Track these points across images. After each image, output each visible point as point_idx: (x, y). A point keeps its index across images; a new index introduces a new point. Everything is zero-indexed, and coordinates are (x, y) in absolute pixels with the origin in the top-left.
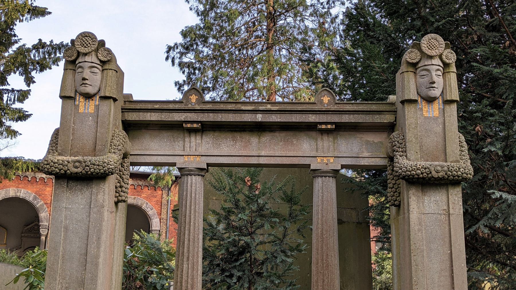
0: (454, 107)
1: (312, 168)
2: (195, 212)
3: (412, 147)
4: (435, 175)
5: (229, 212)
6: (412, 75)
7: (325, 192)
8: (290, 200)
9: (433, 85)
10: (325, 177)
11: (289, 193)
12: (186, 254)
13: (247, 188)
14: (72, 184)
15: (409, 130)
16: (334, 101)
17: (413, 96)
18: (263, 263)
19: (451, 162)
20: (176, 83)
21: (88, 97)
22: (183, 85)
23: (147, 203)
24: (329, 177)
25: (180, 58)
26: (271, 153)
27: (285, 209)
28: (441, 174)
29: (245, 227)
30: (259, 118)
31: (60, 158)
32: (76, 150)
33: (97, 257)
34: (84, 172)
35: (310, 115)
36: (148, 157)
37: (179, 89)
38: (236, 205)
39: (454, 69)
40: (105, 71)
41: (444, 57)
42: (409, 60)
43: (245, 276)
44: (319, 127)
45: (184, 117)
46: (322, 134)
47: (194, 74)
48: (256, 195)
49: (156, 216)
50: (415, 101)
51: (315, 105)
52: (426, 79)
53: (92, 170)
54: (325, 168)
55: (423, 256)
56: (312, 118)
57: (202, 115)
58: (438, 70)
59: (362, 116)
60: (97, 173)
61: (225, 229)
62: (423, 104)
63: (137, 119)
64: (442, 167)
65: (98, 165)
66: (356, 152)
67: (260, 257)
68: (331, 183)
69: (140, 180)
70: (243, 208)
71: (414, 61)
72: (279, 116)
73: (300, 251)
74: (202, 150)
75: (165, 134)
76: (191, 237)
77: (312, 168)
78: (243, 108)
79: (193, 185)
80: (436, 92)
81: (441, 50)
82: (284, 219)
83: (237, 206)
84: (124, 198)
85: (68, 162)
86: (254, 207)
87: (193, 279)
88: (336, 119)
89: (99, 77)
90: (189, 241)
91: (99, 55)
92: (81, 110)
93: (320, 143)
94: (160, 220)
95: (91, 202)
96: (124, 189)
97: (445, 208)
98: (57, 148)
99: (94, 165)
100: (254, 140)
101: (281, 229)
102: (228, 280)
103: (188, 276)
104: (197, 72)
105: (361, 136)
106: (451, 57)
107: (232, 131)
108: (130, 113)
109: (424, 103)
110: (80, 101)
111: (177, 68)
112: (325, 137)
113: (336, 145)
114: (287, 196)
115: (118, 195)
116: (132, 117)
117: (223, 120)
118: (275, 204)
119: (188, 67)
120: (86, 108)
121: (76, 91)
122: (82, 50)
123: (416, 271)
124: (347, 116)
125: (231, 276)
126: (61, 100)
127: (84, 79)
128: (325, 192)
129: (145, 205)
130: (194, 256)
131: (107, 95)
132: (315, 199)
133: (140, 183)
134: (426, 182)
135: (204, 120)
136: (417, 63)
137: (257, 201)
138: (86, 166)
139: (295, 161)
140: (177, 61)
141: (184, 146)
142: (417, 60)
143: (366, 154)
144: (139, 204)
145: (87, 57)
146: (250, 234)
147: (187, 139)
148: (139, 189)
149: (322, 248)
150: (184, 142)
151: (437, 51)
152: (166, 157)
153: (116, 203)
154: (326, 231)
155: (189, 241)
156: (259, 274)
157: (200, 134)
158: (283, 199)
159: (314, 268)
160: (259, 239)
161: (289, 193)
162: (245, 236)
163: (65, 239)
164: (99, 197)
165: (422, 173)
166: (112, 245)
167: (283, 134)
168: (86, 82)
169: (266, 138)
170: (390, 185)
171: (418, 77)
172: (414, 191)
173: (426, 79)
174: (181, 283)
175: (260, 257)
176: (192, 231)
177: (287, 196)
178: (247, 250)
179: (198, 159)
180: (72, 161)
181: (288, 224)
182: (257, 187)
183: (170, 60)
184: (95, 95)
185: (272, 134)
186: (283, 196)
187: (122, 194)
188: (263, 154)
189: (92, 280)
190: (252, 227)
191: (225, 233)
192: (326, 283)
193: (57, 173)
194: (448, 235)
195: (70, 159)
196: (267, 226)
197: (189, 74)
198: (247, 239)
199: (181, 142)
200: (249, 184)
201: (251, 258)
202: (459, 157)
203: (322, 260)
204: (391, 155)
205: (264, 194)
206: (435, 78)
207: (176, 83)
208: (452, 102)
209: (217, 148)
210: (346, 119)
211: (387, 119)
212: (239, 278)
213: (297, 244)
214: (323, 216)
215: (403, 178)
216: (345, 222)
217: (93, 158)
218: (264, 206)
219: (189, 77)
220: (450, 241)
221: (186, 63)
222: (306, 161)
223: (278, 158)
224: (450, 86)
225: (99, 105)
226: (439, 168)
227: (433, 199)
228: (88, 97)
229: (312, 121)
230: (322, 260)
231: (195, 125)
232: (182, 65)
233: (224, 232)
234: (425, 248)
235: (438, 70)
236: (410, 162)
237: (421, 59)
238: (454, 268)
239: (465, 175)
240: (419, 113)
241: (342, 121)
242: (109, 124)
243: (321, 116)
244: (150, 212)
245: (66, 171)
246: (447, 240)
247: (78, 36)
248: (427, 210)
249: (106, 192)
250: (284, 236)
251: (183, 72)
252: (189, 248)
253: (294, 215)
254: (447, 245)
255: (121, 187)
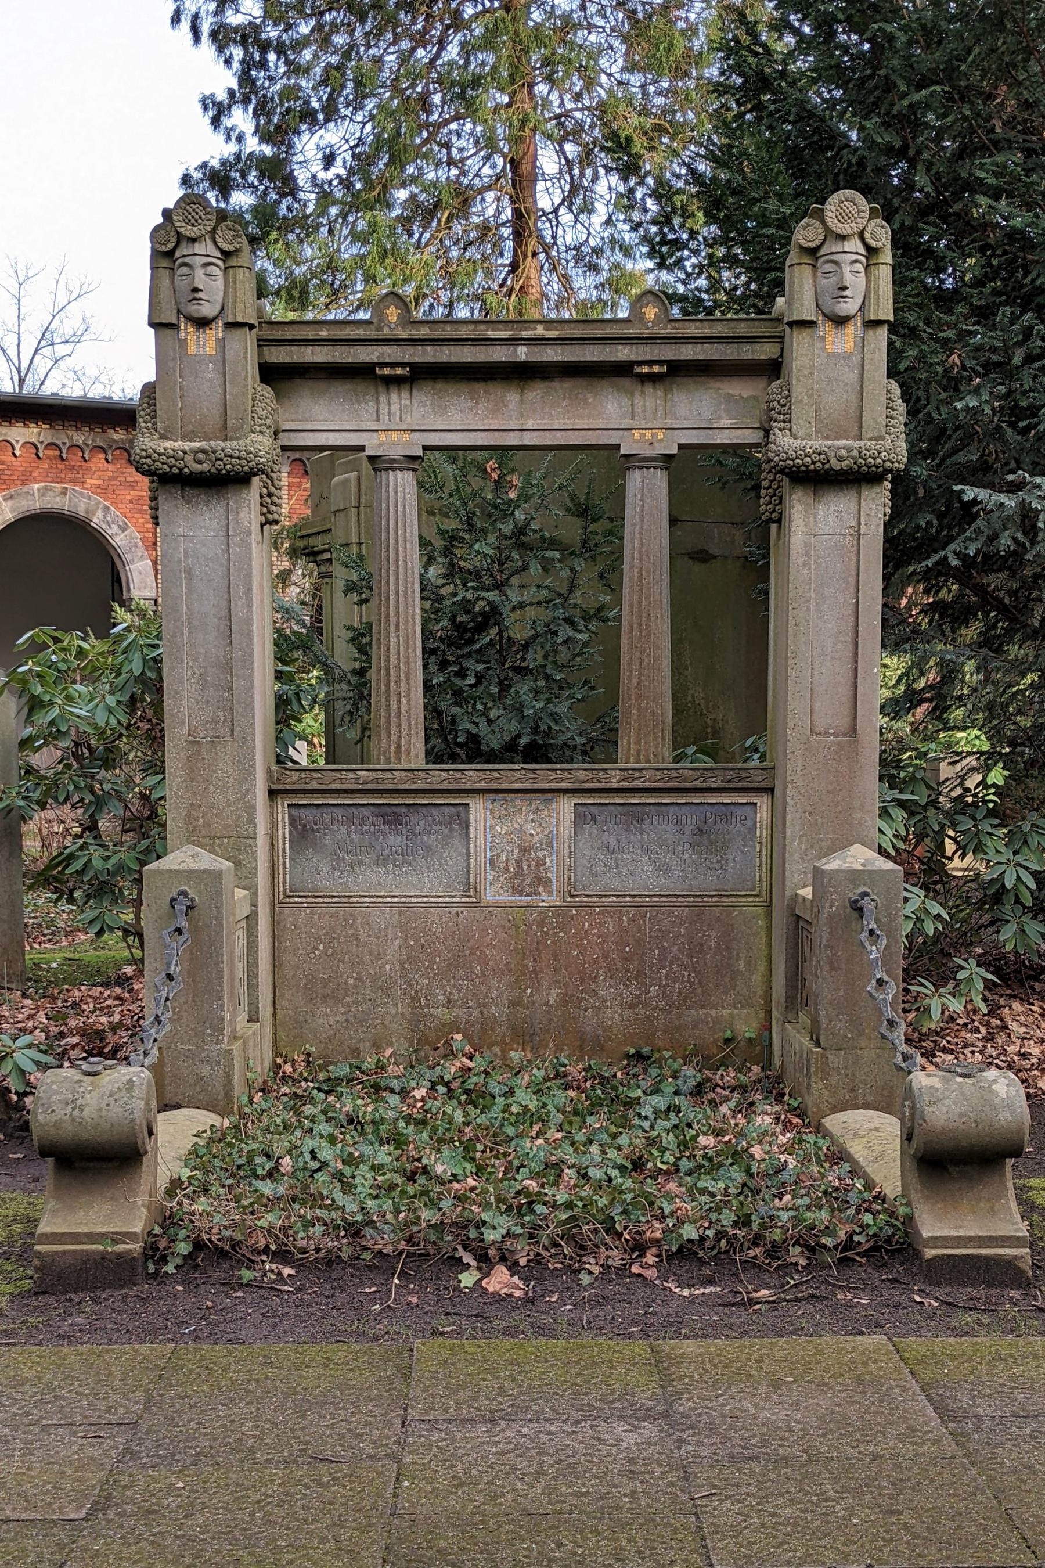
0: (883, 332)
1: (623, 451)
2: (405, 541)
3: (802, 414)
4: (836, 465)
5: (453, 538)
6: (807, 270)
7: (647, 497)
8: (583, 511)
9: (845, 293)
10: (648, 468)
11: (583, 499)
12: (393, 620)
13: (491, 485)
14: (190, 492)
15: (798, 380)
16: (666, 316)
17: (808, 313)
18: (526, 647)
19: (870, 439)
20: (207, 102)
21: (202, 323)
22: (230, 107)
23: (106, 509)
24: (655, 468)
25: (216, 14)
26: (546, 423)
27: (571, 530)
28: (846, 462)
29: (488, 570)
30: (522, 353)
31: (168, 444)
32: (190, 428)
33: (249, 622)
34: (213, 470)
35: (620, 347)
36: (311, 434)
37: (216, 122)
38: (469, 524)
39: (887, 257)
40: (231, 271)
41: (867, 235)
42: (802, 242)
43: (490, 672)
44: (638, 370)
45: (377, 354)
46: (642, 383)
47: (263, 65)
48: (511, 500)
49: (141, 550)
50: (811, 324)
51: (629, 325)
52: (833, 280)
53: (228, 467)
54: (647, 451)
55: (809, 609)
56: (623, 353)
57: (411, 350)
58: (856, 261)
59: (720, 346)
60: (238, 473)
61: (445, 576)
62: (826, 328)
63: (288, 360)
64: (849, 450)
65: (239, 458)
66: (706, 416)
67: (519, 633)
68: (659, 480)
69: (78, 429)
70: (484, 531)
71: (812, 245)
72: (559, 349)
73: (605, 620)
74: (412, 420)
75: (342, 387)
76: (401, 588)
77: (623, 451)
78: (491, 334)
79: (400, 489)
80: (849, 306)
81: (861, 223)
82: (572, 553)
83: (471, 527)
84: (276, 516)
85: (185, 453)
86: (507, 528)
87: (407, 663)
88: (669, 353)
89: (220, 282)
90: (397, 594)
91: (218, 239)
92: (192, 349)
93: (638, 401)
94: (155, 563)
95: (228, 524)
96: (275, 499)
97: (854, 523)
98: (155, 424)
99: (231, 457)
100: (512, 397)
101: (565, 574)
102: (457, 681)
103: (398, 659)
104: (272, 57)
105: (718, 385)
106: (881, 234)
107: (469, 379)
108: (273, 349)
109: (829, 326)
110: (188, 332)
111: (207, 47)
112: (649, 389)
113: (669, 404)
114: (577, 504)
115: (265, 510)
116: (279, 356)
117: (453, 359)
118: (555, 521)
119: (243, 42)
120: (202, 345)
121: (179, 312)
122: (187, 231)
123: (795, 636)
124: (690, 346)
125: (462, 674)
126: (152, 331)
127: (196, 290)
128: (647, 497)
129: (100, 513)
130: (407, 621)
131: (240, 319)
132: (628, 512)
133: (79, 438)
134: (821, 479)
135: (417, 360)
136: (818, 248)
137: (513, 513)
138: (218, 459)
139: (591, 438)
140: (205, 29)
141: (377, 411)
142: (817, 243)
143: (726, 422)
144: (81, 511)
145: (197, 245)
146: (498, 586)
147: (383, 398)
148: (75, 460)
149: (640, 603)
150: (378, 403)
151: (853, 225)
152: (344, 434)
153: (262, 525)
154: (648, 572)
155: (397, 594)
156: (521, 671)
157: (407, 386)
158: (568, 510)
159: (624, 640)
160: (515, 597)
161: (583, 499)
162: (488, 590)
163: (189, 592)
164: (242, 515)
165: (814, 463)
166: (262, 601)
167: (568, 384)
168: (200, 295)
169: (536, 392)
170: (765, 483)
171: (819, 274)
172: (800, 494)
173: (833, 280)
174: (388, 669)
175: (519, 633)
176: (401, 576)
177: (577, 504)
178: (492, 621)
179: (406, 437)
180: (191, 450)
181: (579, 564)
182: (511, 482)
183: (185, 25)
184: (215, 318)
185: (547, 384)
186: (570, 504)
187: (273, 508)
188: (529, 426)
189: (244, 661)
190: (501, 572)
191: (443, 585)
192: (645, 664)
193: (165, 473)
194: (854, 573)
195: (188, 445)
196: (535, 569)
197: (247, 64)
198: (492, 596)
199: (371, 404)
200: (495, 476)
201: (501, 638)
202: (883, 429)
203: (640, 625)
204: (766, 426)
205: (527, 498)
206: (848, 279)
207: (207, 102)
208: (878, 323)
209: (442, 415)
210: (688, 353)
211: (765, 352)
212: (479, 678)
213: (597, 605)
214: (642, 544)
215: (782, 471)
216: (715, 557)
217: (228, 443)
218: (528, 524)
219: (245, 78)
220: (858, 581)
221: (236, 29)
222: (611, 439)
223: (559, 434)
224: (877, 292)
225: (224, 339)
226: (844, 453)
227: (832, 508)
228: (202, 323)
229: (624, 358)
230: (640, 625)
231: (399, 371)
232: (222, 37)
233: (440, 582)
234: (813, 595)
235: (856, 261)
236: (797, 442)
237: (822, 244)
238: (860, 628)
239: (888, 464)
240: (818, 345)
241: (682, 358)
242: (246, 376)
243: (641, 347)
244: (119, 539)
245: (181, 470)
246: (852, 581)
247: (178, 202)
248: (822, 528)
249: (247, 507)
250: (571, 589)
251: (228, 62)
252: (397, 607)
253: (592, 543)
254: (852, 589)
255: (270, 495)
